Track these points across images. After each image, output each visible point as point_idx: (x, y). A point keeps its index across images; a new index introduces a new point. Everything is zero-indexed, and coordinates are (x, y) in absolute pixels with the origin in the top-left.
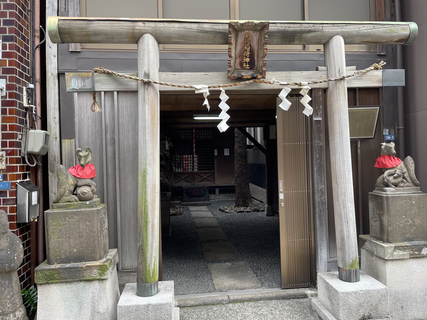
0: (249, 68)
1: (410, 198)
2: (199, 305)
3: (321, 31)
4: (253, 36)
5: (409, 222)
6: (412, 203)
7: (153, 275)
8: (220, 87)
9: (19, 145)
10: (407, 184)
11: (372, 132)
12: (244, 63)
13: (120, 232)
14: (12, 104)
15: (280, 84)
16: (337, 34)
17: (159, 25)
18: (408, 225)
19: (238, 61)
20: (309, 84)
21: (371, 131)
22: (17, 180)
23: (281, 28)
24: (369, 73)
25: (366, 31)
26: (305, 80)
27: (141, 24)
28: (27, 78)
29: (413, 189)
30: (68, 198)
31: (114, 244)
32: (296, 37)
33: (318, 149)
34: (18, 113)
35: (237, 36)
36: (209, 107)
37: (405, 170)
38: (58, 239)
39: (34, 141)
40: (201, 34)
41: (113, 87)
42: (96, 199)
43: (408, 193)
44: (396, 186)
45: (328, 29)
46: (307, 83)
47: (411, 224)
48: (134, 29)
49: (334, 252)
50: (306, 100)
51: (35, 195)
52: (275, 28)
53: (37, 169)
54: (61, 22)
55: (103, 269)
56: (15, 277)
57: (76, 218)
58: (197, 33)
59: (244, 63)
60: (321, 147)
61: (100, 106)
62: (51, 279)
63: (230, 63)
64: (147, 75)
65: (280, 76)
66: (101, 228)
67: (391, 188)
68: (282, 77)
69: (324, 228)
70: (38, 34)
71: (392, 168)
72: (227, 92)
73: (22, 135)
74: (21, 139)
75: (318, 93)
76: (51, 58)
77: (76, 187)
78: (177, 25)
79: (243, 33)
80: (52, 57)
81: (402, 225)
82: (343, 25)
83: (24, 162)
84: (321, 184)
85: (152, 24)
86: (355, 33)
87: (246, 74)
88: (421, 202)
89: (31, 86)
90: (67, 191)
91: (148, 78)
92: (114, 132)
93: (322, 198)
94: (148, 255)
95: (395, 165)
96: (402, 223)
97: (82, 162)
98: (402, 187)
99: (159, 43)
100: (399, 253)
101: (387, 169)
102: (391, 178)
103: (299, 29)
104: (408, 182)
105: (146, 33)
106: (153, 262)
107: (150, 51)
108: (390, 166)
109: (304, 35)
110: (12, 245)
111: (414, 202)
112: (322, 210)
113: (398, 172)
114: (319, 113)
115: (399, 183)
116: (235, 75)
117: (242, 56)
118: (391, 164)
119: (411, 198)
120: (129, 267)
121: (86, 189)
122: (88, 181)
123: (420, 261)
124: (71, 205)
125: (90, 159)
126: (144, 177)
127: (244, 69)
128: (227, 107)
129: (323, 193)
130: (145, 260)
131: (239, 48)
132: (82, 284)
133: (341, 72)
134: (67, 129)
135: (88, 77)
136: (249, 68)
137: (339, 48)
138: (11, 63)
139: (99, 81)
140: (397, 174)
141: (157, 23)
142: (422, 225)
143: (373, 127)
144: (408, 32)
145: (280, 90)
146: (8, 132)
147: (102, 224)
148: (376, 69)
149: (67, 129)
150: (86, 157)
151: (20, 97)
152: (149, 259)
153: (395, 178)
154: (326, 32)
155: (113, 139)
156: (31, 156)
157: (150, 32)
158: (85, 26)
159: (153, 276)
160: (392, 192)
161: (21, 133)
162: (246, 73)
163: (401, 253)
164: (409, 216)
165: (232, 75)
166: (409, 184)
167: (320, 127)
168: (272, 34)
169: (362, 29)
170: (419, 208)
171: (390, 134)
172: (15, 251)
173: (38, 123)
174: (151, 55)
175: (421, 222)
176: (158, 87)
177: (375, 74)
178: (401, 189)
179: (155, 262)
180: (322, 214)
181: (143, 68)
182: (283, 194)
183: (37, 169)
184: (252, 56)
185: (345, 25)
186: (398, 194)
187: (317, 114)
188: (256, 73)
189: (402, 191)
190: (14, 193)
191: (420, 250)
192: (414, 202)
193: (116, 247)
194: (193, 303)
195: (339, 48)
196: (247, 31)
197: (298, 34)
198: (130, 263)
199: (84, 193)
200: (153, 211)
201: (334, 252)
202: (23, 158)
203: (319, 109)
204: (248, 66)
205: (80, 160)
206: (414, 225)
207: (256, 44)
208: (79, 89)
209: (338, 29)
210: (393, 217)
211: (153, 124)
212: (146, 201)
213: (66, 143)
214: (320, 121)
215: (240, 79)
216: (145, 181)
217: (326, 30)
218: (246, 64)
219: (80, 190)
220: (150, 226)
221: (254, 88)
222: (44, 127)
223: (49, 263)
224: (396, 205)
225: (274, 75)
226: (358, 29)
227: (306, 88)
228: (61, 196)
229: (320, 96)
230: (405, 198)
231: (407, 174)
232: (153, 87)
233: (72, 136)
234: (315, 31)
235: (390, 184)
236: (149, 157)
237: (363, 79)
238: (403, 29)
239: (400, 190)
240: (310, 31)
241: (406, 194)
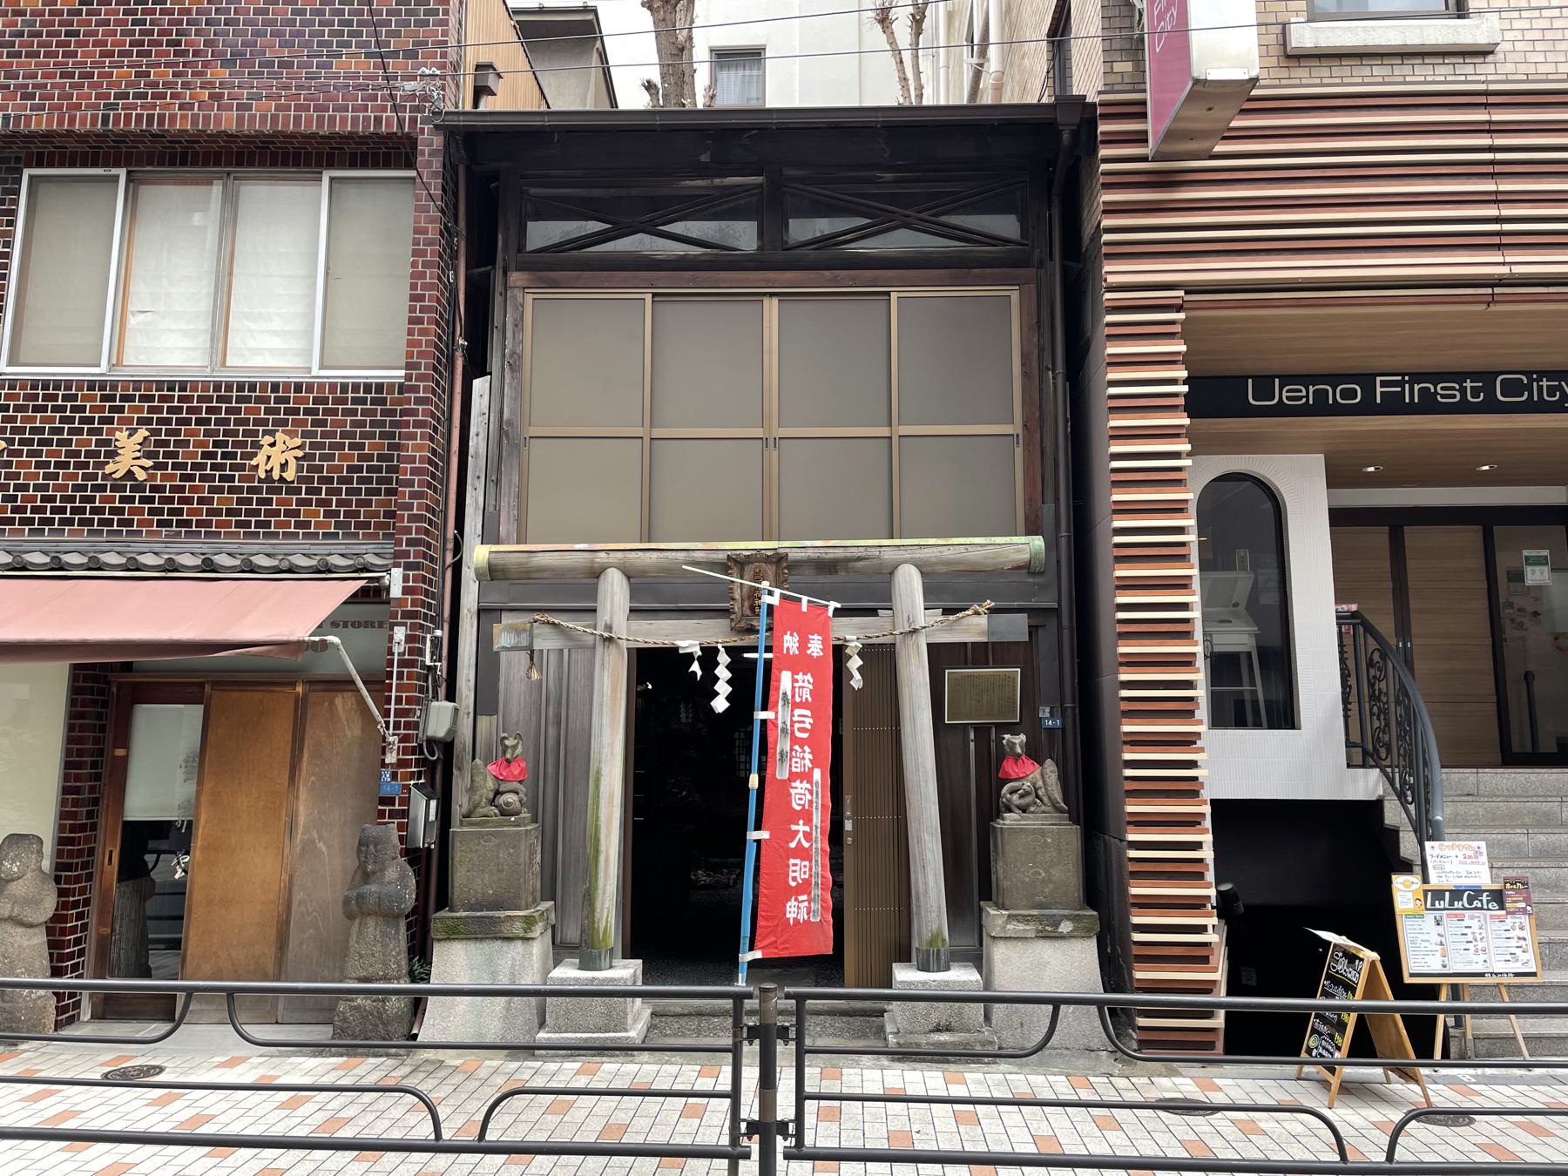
1: (1043, 833)
2: (690, 1015)
3: (878, 558)
9: (416, 726)
13: (560, 877)
14: (412, 664)
16: (906, 562)
17: (629, 555)
24: (964, 621)
27: (603, 555)
28: (433, 620)
30: (485, 810)
31: (550, 892)
34: (419, 677)
36: (699, 673)
37: (1040, 783)
38: (465, 876)
39: (438, 719)
42: (525, 815)
50: (855, 663)
51: (433, 804)
53: (438, 764)
55: (529, 922)
56: (403, 924)
57: (496, 841)
61: (540, 671)
62: (455, 933)
64: (609, 628)
66: (531, 860)
70: (450, 546)
72: (729, 650)
77: (498, 793)
78: (655, 555)
83: (421, 753)
85: (619, 555)
89: (438, 633)
92: (559, 704)
94: (598, 904)
97: (508, 756)
99: (629, 578)
100: (1014, 928)
102: (1015, 797)
107: (615, 593)
108: (1014, 776)
110: (403, 876)
113: (1027, 785)
115: (1028, 805)
116: (742, 624)
121: (510, 798)
122: (515, 785)
123: (1057, 944)
125: (519, 750)
126: (598, 780)
128: (728, 675)
130: (593, 911)
132: (499, 943)
134: (486, 701)
137: (909, 585)
138: (414, 603)
139: (539, 635)
144: (1027, 556)
146: (404, 706)
147: (532, 854)
148: (977, 613)
149: (486, 701)
150: (515, 747)
151: (421, 652)
153: (1022, 796)
155: (558, 716)
156: (431, 741)
163: (1021, 927)
170: (1059, 850)
171: (1051, 713)
172: (406, 887)
173: (442, 691)
174: (616, 598)
176: (624, 645)
181: (603, 617)
183: (438, 764)
190: (406, 801)
191: (1057, 925)
193: (553, 898)
194: (678, 1010)
195: (909, 585)
198: (572, 934)
199: (508, 804)
200: (608, 836)
202: (421, 746)
205: (504, 753)
206: (1051, 881)
211: (614, 699)
212: (597, 819)
213: (484, 721)
216: (597, 787)
219: (502, 799)
220: (602, 858)
222: (451, 696)
223: (451, 910)
227: (854, 645)
228: (476, 806)
233: (493, 711)
236: (606, 750)
238: (1018, 551)
240: (859, 559)
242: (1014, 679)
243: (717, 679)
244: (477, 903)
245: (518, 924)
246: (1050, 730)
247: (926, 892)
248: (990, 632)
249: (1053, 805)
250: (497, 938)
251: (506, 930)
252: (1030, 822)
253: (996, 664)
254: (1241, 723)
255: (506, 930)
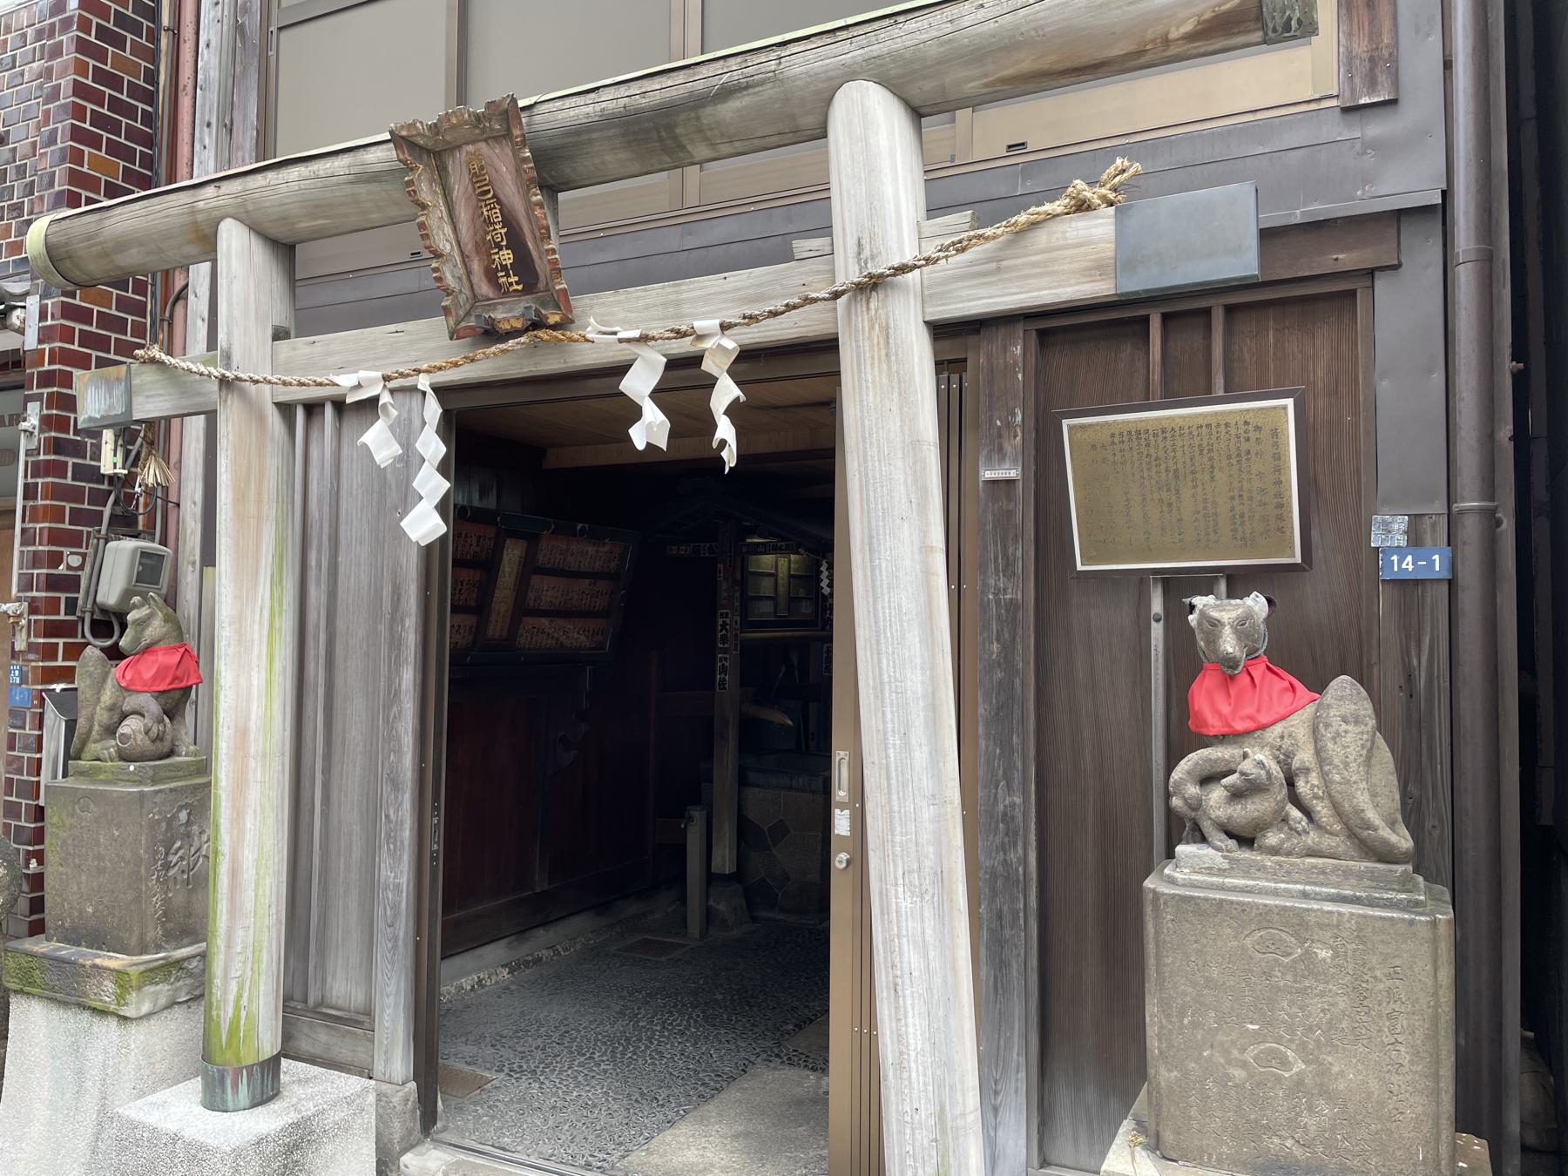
0: (520, 287)
1: (1299, 924)
3: (775, 78)
4: (496, 160)
5: (1285, 1063)
6: (1308, 956)
7: (230, 1038)
8: (418, 371)
10: (1312, 838)
11: (1283, 529)
12: (497, 270)
15: (621, 341)
16: (851, 74)
18: (1279, 1079)
19: (476, 266)
20: (724, 327)
21: (1281, 530)
22: (52, 683)
23: (610, 105)
24: (1041, 237)
25: (992, 25)
26: (718, 314)
29: (1347, 873)
32: (679, 130)
33: (999, 616)
35: (441, 173)
40: (362, 189)
41: (168, 405)
43: (1305, 895)
44: (1246, 840)
45: (803, 63)
46: (714, 323)
47: (1299, 1082)
48: (193, 212)
49: (1076, 1140)
52: (589, 109)
54: (55, 228)
58: (349, 189)
59: (497, 270)
60: (1013, 606)
63: (439, 279)
65: (641, 303)
67: (1210, 851)
68: (647, 308)
69: (1017, 1009)
71: (1229, 737)
73: (84, 556)
74: (81, 567)
75: (1005, 349)
76: (195, 324)
79: (461, 156)
80: (199, 322)
81: (1238, 1073)
82: (867, 28)
84: (1009, 786)
86: (933, 51)
87: (507, 314)
88: (1374, 960)
90: (96, 727)
91: (228, 366)
93: (1012, 856)
95: (1248, 725)
96: (1244, 1065)
98: (1274, 851)
101: (1204, 742)
102: (1217, 794)
103: (682, 90)
104: (1320, 827)
105: (222, 218)
106: (232, 997)
109: (708, 114)
111: (1324, 954)
112: (1007, 918)
113: (1257, 758)
114: (1008, 448)
115: (1261, 826)
117: (485, 248)
118: (1220, 714)
119: (1303, 924)
120: (341, 1003)
124: (99, 770)
127: (507, 294)
129: (1016, 833)
131: (463, 216)
132: (87, 1014)
133: (866, 253)
135: (118, 379)
136: (520, 287)
140: (1242, 774)
141: (249, 178)
142: (1382, 1104)
143: (1283, 506)
145: (622, 370)
148: (1082, 206)
152: (218, 982)
153: (1236, 795)
154: (795, 78)
156: (104, 610)
157: (231, 211)
158: (93, 228)
159: (229, 1044)
160: (1210, 871)
161: (83, 550)
162: (510, 310)
164: (1291, 1030)
165: (463, 324)
166: (1328, 842)
167: (1010, 514)
168: (586, 137)
169: (966, 22)
171: (1415, 539)
175: (1374, 1085)
177: (1071, 234)
178: (1269, 861)
179: (239, 996)
180: (1007, 933)
182: (847, 812)
184: (515, 241)
185: (887, 22)
186: (1234, 889)
187: (1001, 448)
188: (544, 305)
189: (1273, 875)
192: (1324, 954)
196: (470, 148)
197: (683, 116)
201: (1076, 1140)
203: (1009, 425)
204: (514, 279)
207: (514, 189)
208: (103, 417)
209: (849, 52)
210: (1182, 1014)
214: (1010, 482)
215: (491, 334)
217: (797, 70)
218: (508, 275)
221: (550, 364)
224: (1200, 953)
225: (619, 302)
226: (949, 28)
229: (1015, 364)
230: (1265, 917)
231: (1314, 778)
232: (243, 395)
234: (748, 87)
235: (1207, 826)
237: (1010, 269)
239: (1262, 868)
240: (727, 92)
241: (1290, 894)
242: (1277, 433)
243: (443, 469)
244: (74, 929)
245: (109, 986)
246: (1408, 586)
247: (901, 1066)
248: (1125, 260)
249: (1352, 834)
250: (85, 1007)
251: (106, 992)
252: (1261, 883)
253: (1234, 393)
254: (826, 1061)
255: (106, 992)
